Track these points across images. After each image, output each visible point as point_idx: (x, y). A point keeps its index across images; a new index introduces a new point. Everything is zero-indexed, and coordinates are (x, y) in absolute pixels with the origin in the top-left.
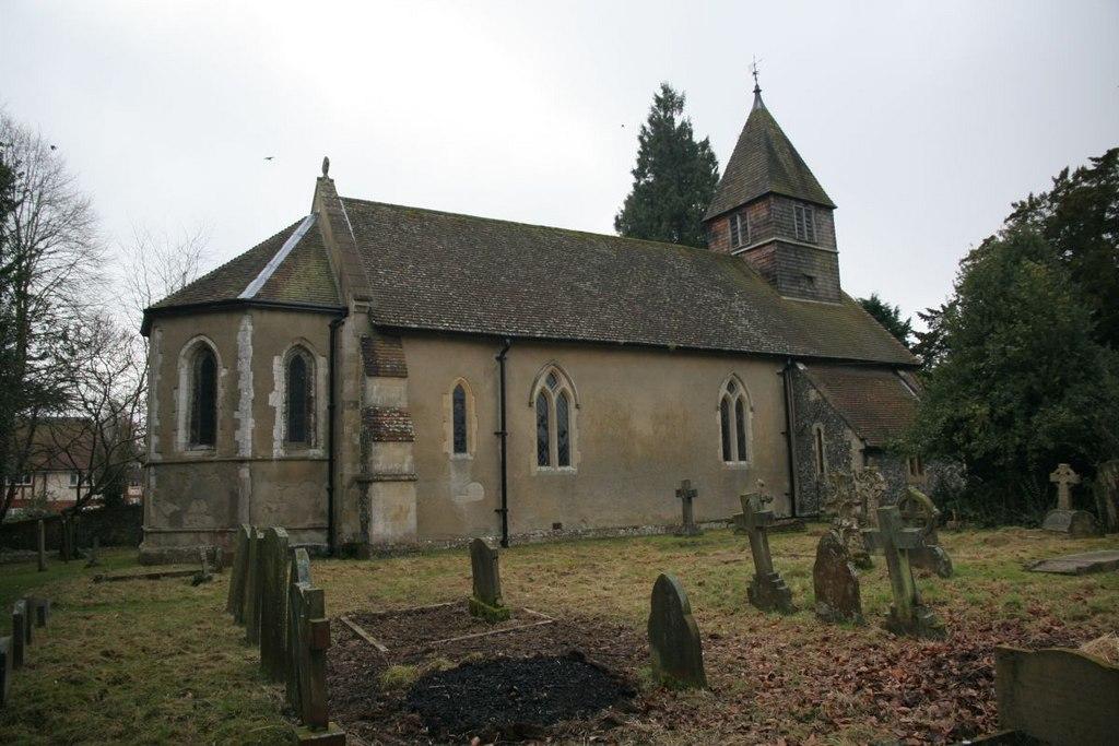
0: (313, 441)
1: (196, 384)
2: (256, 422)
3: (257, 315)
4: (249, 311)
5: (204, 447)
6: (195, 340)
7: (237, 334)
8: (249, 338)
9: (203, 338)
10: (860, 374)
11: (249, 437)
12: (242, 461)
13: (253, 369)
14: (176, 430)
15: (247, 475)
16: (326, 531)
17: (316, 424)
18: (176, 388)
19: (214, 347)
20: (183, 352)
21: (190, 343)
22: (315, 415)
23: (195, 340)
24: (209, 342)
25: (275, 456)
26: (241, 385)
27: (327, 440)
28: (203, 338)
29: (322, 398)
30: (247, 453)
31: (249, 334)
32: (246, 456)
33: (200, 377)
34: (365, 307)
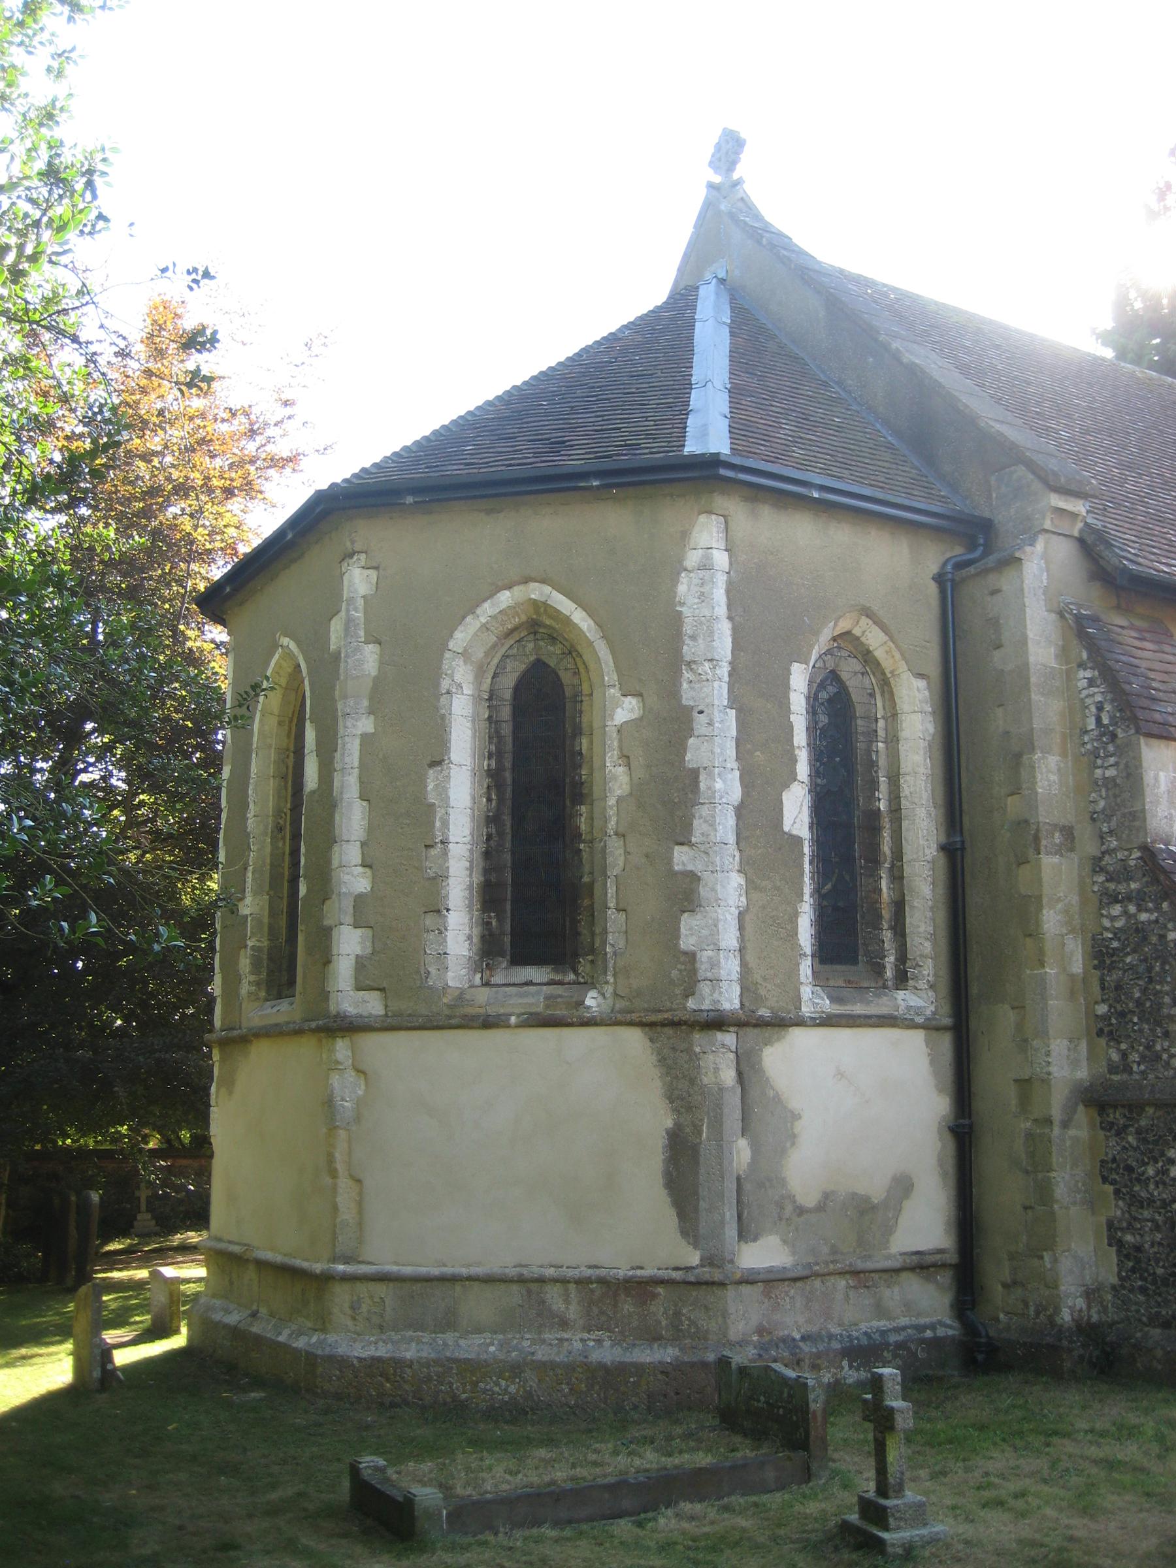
0: (890, 960)
1: (496, 754)
2: (751, 886)
3: (734, 506)
4: (722, 502)
5: (538, 974)
6: (505, 598)
7: (675, 581)
8: (719, 595)
9: (537, 591)
10: (395, 1268)
11: (730, 938)
12: (717, 1023)
13: (735, 701)
14: (438, 910)
15: (728, 1076)
16: (945, 1278)
17: (899, 906)
18: (437, 763)
19: (580, 618)
20: (461, 638)
21: (487, 610)
22: (898, 877)
23: (505, 598)
24: (563, 604)
25: (806, 1010)
26: (695, 754)
27: (944, 957)
28: (537, 591)
29: (921, 813)
30: (730, 999)
31: (721, 580)
32: (726, 1006)
33: (507, 730)
34: (1074, 516)
